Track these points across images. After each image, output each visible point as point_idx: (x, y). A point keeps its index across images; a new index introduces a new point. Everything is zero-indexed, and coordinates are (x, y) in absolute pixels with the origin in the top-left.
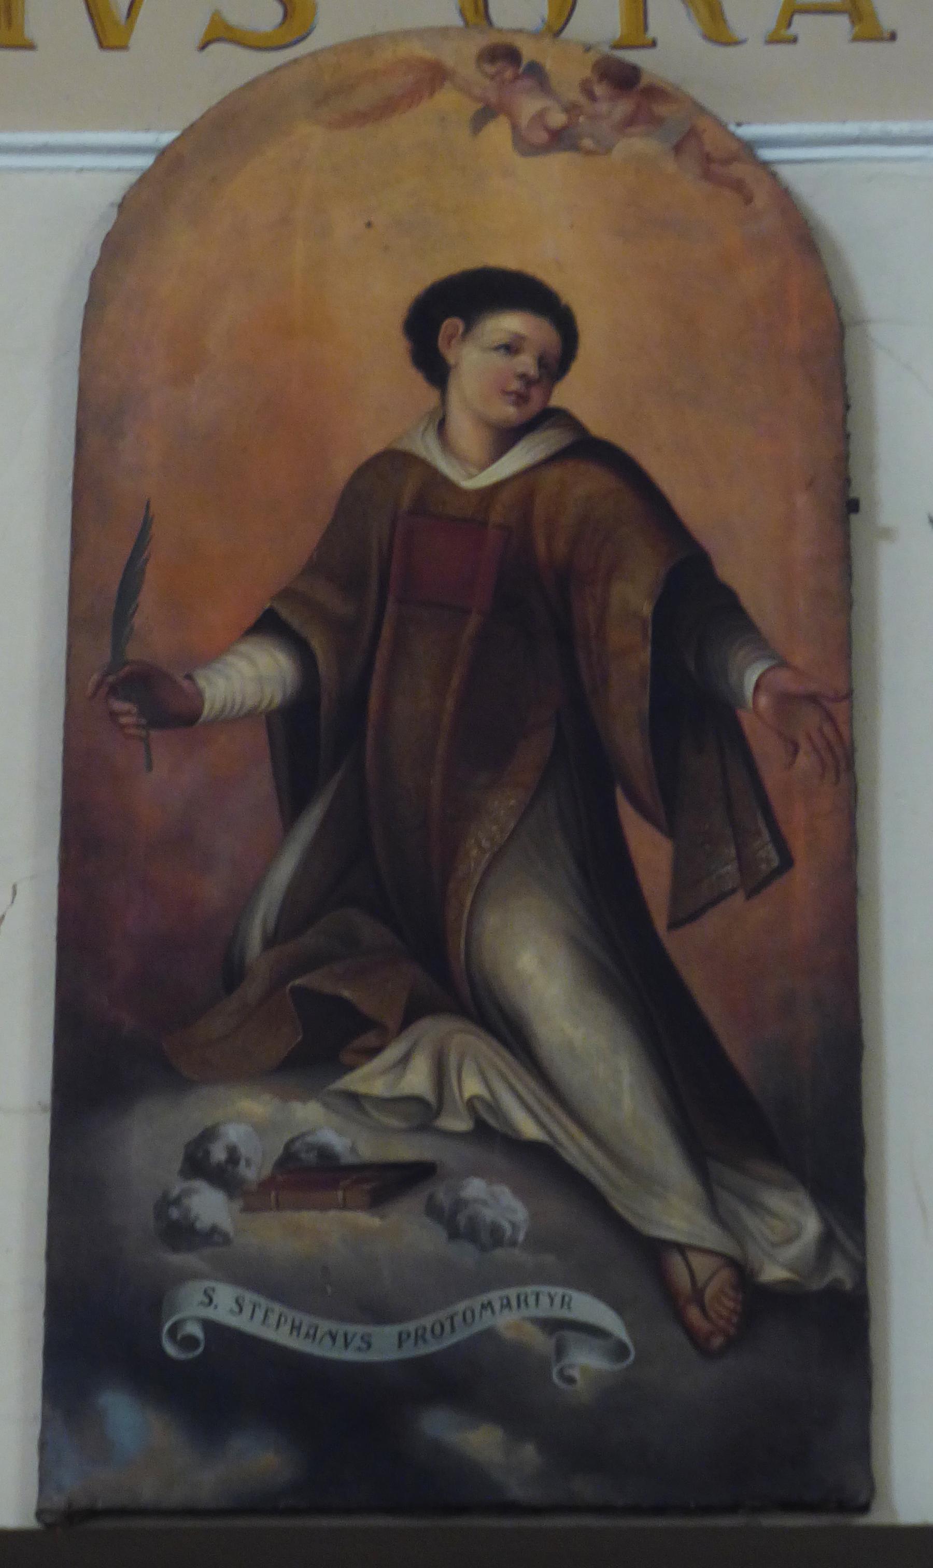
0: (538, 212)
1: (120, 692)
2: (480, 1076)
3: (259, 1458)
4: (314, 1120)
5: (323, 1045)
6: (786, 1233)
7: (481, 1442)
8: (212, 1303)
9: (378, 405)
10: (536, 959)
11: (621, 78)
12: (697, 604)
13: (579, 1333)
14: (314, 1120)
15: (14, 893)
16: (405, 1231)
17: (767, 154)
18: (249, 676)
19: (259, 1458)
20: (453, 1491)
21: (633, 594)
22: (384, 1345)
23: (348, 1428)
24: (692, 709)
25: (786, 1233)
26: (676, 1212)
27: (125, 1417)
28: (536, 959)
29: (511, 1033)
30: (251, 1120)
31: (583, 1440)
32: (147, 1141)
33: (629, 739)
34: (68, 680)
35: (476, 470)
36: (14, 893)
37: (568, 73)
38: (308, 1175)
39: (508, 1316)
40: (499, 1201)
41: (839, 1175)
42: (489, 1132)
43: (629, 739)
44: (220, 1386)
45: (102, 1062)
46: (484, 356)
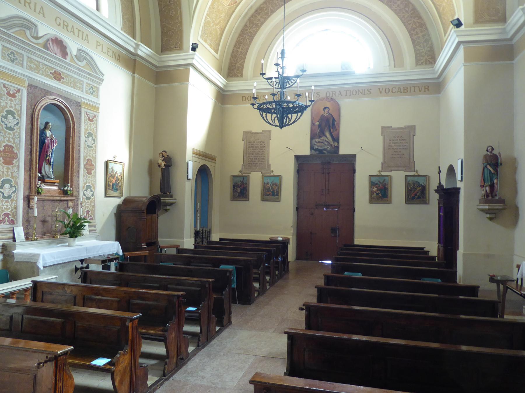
0: (328, 105)
1: (313, 124)
2: (325, 139)
3: (317, 152)
4: (319, 140)
5: (320, 137)
6: (336, 144)
7: (325, 152)
8: (316, 147)
9: (322, 112)
10: (327, 134)
11: (332, 99)
12: (334, 120)
13: (329, 148)
14: (319, 140)
15: (327, 30)
16: (323, 144)
17: (299, 114)
18: (317, 123)
19: (317, 152)
20: (324, 153)
21: (331, 120)
22: (322, 148)
23: (320, 151)
24: (333, 124)
25: (336, 144)
26: (332, 143)
27: (313, 151)
28: (327, 134)
29: (326, 137)
30: (317, 140)
31: (329, 152)
32: (314, 141)
33: (331, 125)
34: (297, 224)
35: (326, 115)
36: (327, 30)
37: (330, 98)
38: (319, 142)
39: (326, 147)
40: (326, 143)
41: (338, 142)
42: (326, 141)
43: (331, 125)
44: (316, 150)
45: (312, 138)
46: (326, 110)
